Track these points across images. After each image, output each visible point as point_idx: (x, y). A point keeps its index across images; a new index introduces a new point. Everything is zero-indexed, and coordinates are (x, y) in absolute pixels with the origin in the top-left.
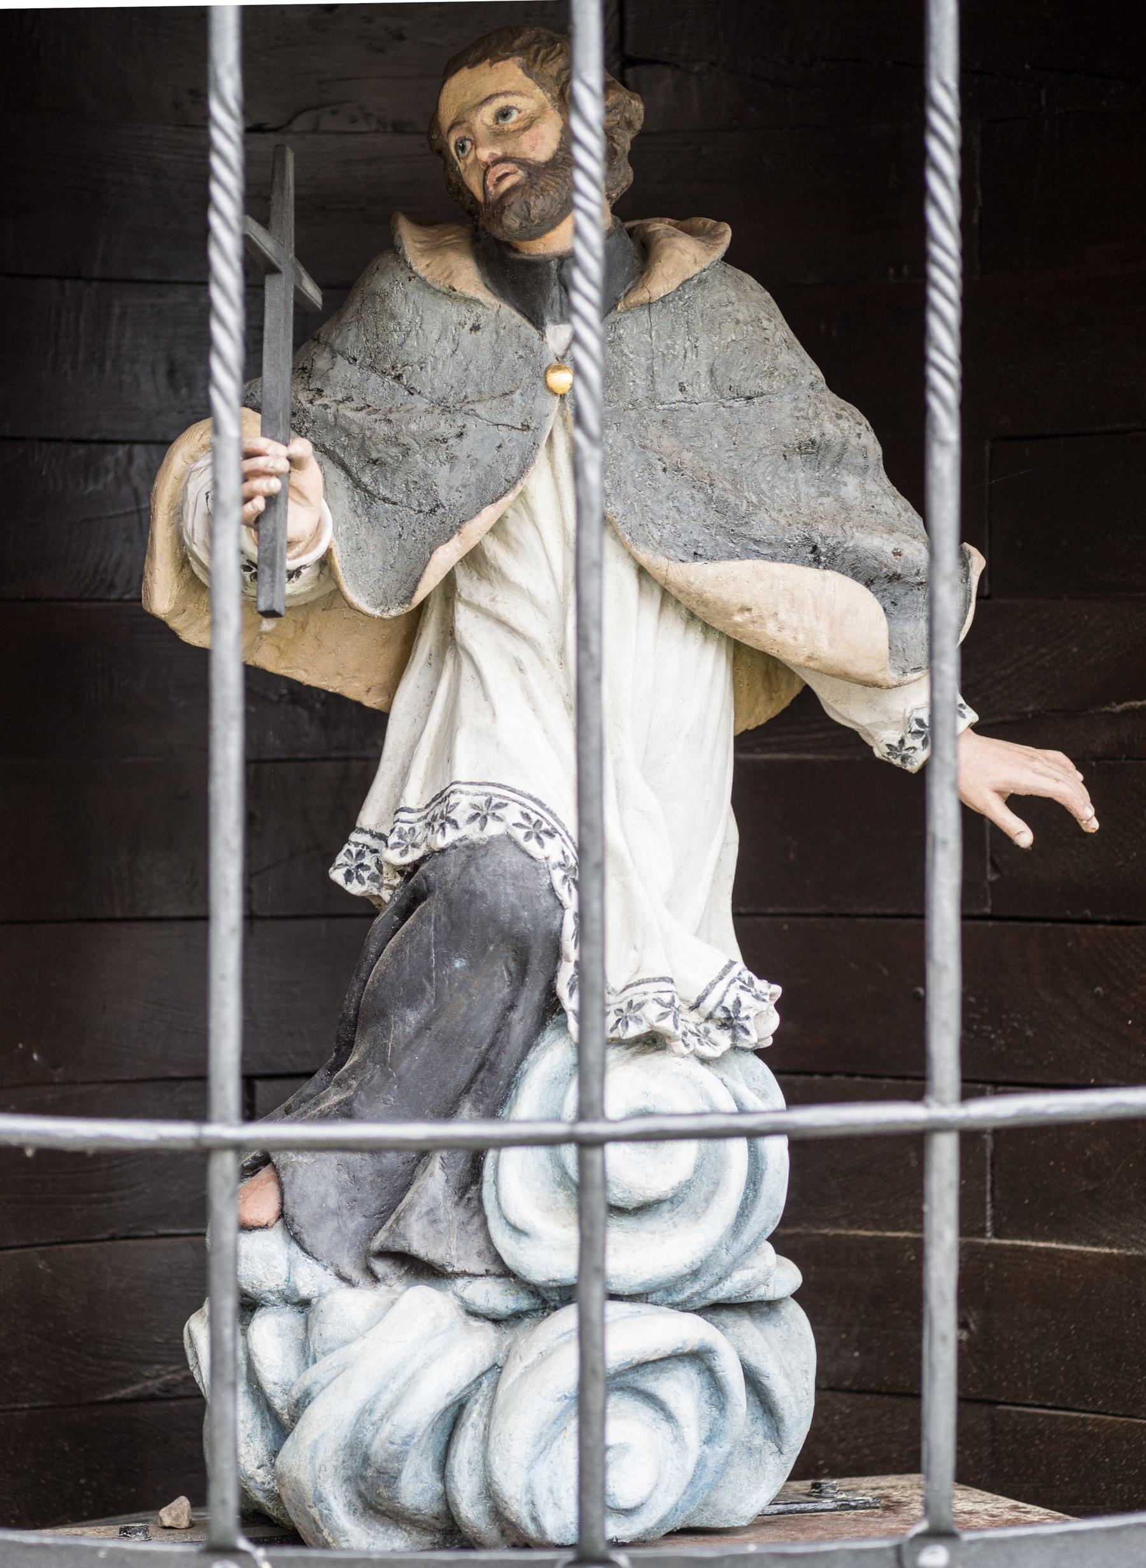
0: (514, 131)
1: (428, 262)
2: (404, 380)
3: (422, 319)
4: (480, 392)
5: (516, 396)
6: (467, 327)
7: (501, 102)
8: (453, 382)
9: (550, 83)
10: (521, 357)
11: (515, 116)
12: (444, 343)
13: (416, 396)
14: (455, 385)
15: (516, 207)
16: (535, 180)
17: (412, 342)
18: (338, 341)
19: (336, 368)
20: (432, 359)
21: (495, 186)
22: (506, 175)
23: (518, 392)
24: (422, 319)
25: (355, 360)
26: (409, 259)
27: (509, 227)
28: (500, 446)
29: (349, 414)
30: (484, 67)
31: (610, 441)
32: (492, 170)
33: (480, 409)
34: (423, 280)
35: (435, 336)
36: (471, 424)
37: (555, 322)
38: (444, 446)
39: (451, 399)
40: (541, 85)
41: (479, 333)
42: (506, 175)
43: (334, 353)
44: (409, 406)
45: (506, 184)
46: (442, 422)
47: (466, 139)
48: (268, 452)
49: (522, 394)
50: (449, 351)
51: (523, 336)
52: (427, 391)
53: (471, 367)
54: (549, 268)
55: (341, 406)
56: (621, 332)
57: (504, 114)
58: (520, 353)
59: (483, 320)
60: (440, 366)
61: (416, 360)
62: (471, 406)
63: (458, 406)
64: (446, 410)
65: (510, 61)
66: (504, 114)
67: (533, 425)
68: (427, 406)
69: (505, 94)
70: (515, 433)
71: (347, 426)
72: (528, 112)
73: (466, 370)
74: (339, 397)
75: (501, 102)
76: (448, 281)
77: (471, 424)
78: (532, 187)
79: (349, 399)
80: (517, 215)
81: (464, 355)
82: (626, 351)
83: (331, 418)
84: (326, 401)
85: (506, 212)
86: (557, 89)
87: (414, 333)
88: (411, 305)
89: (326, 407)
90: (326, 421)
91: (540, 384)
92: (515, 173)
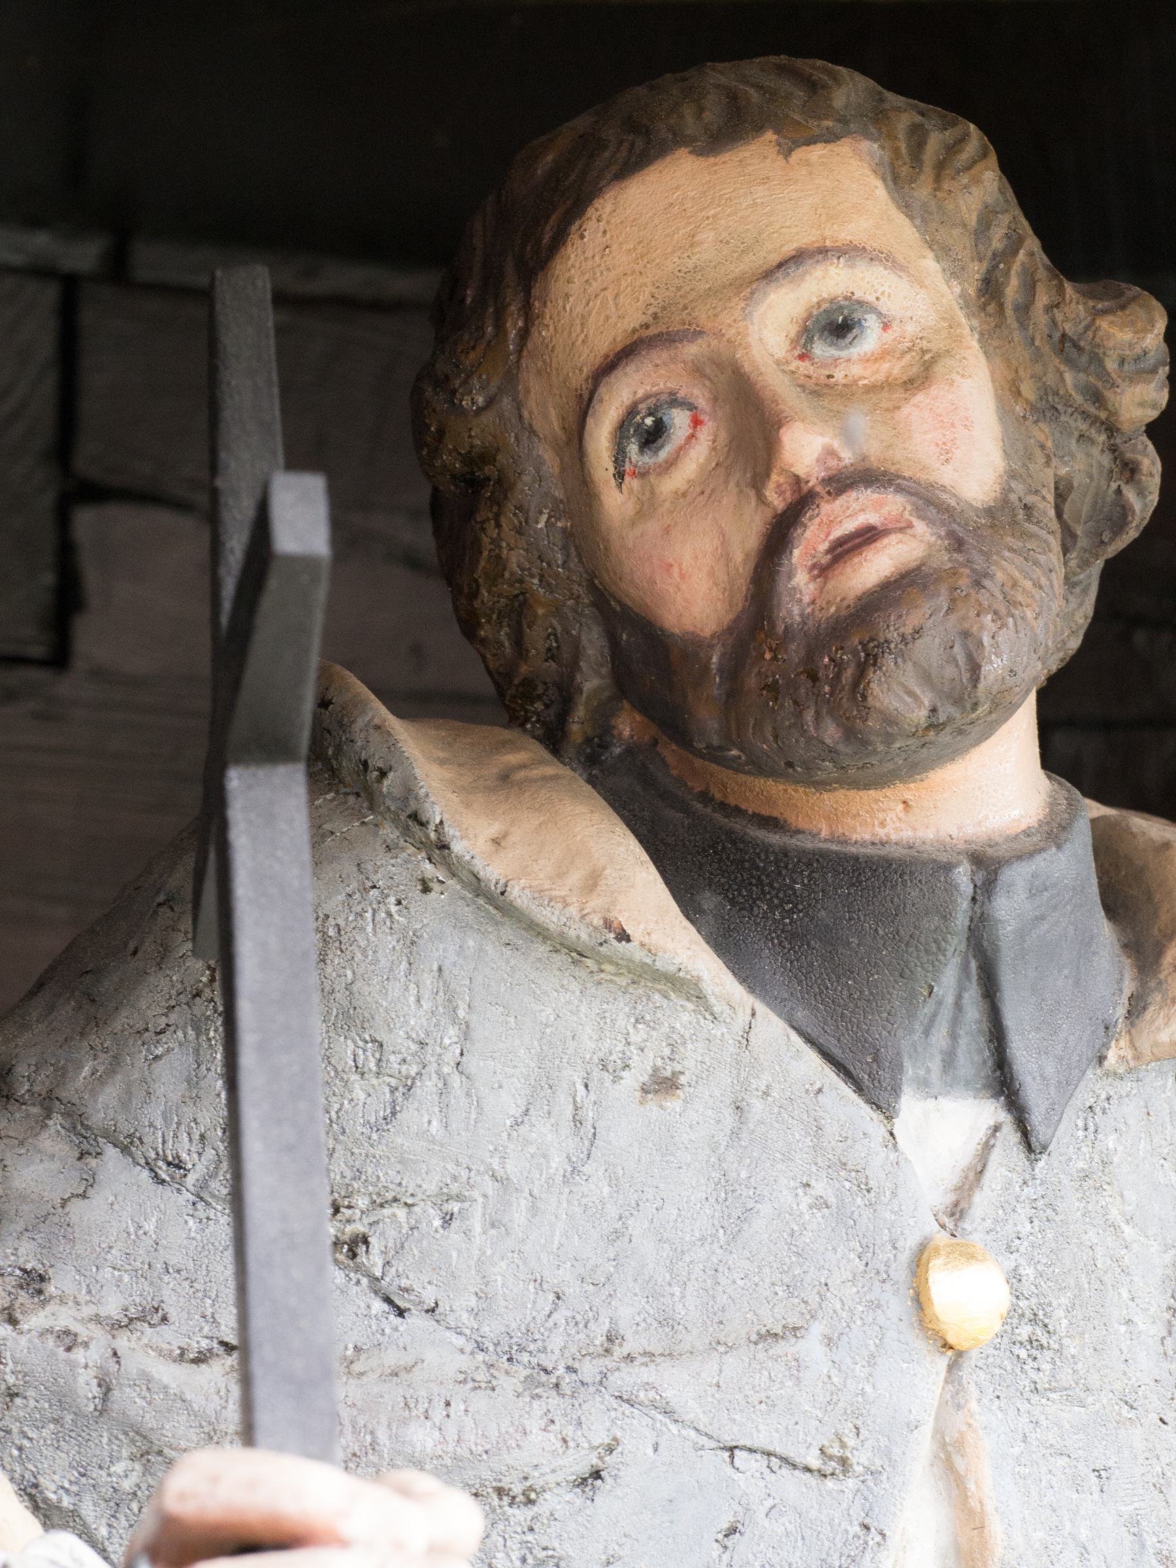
0: (872, 389)
1: (495, 829)
2: (374, 1260)
3: (466, 1033)
4: (667, 1322)
5: (811, 1346)
6: (633, 1079)
7: (828, 282)
8: (563, 1276)
9: (960, 241)
10: (821, 1204)
11: (871, 339)
12: (541, 1131)
13: (416, 1320)
14: (572, 1290)
15: (929, 649)
16: (980, 563)
17: (421, 1114)
18: (110, 1094)
19: (100, 1198)
20: (490, 1187)
21: (822, 572)
22: (868, 536)
23: (817, 1329)
24: (466, 1033)
25: (177, 1164)
26: (435, 813)
27: (890, 720)
28: (732, 1531)
29: (169, 1374)
30: (757, 156)
31: (1084, 1534)
32: (828, 508)
33: (677, 1384)
34: (476, 886)
35: (508, 1103)
36: (637, 1435)
37: (923, 1084)
38: (520, 1515)
39: (556, 1342)
40: (942, 251)
41: (673, 1104)
42: (868, 536)
43: (87, 1141)
44: (392, 1358)
45: (873, 568)
46: (534, 1425)
47: (675, 401)
48: (347, 1528)
49: (829, 1342)
50: (557, 1162)
51: (831, 1130)
52: (459, 1306)
53: (637, 1227)
54: (951, 888)
55: (123, 1342)
56: (1111, 1141)
57: (838, 324)
58: (820, 1187)
59: (690, 1061)
60: (519, 1215)
61: (431, 1187)
62: (646, 1374)
63: (589, 1370)
64: (542, 1379)
65: (844, 148)
66: (838, 324)
67: (860, 1459)
68: (464, 1362)
69: (849, 252)
70: (791, 1483)
71: (150, 1421)
72: (911, 329)
73: (617, 1235)
74: (112, 1307)
75: (828, 282)
76: (596, 902)
77: (637, 1435)
78: (978, 584)
79: (155, 1315)
80: (926, 678)
81: (614, 1181)
82: (1114, 1214)
83: (86, 1387)
84: (65, 1318)
85: (888, 661)
86: (977, 270)
87: (428, 1087)
88: (428, 980)
89: (69, 1340)
90: (63, 1398)
91: (897, 1306)
92: (905, 528)
